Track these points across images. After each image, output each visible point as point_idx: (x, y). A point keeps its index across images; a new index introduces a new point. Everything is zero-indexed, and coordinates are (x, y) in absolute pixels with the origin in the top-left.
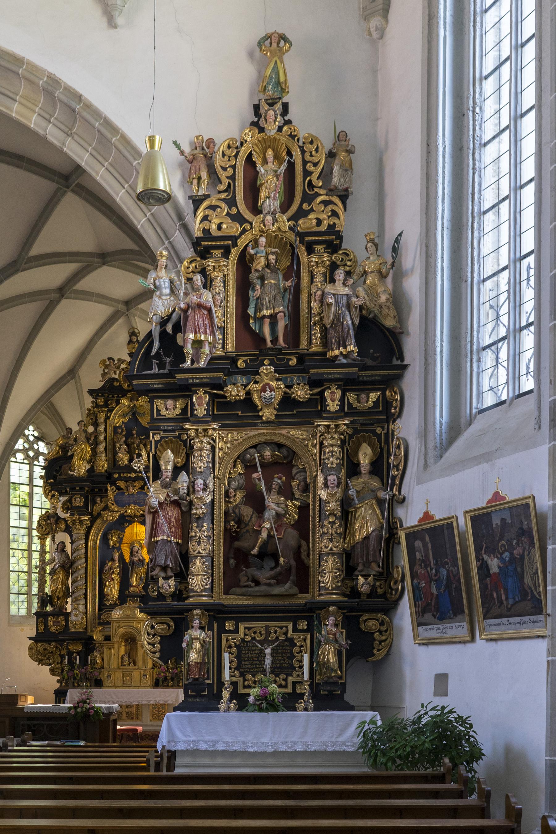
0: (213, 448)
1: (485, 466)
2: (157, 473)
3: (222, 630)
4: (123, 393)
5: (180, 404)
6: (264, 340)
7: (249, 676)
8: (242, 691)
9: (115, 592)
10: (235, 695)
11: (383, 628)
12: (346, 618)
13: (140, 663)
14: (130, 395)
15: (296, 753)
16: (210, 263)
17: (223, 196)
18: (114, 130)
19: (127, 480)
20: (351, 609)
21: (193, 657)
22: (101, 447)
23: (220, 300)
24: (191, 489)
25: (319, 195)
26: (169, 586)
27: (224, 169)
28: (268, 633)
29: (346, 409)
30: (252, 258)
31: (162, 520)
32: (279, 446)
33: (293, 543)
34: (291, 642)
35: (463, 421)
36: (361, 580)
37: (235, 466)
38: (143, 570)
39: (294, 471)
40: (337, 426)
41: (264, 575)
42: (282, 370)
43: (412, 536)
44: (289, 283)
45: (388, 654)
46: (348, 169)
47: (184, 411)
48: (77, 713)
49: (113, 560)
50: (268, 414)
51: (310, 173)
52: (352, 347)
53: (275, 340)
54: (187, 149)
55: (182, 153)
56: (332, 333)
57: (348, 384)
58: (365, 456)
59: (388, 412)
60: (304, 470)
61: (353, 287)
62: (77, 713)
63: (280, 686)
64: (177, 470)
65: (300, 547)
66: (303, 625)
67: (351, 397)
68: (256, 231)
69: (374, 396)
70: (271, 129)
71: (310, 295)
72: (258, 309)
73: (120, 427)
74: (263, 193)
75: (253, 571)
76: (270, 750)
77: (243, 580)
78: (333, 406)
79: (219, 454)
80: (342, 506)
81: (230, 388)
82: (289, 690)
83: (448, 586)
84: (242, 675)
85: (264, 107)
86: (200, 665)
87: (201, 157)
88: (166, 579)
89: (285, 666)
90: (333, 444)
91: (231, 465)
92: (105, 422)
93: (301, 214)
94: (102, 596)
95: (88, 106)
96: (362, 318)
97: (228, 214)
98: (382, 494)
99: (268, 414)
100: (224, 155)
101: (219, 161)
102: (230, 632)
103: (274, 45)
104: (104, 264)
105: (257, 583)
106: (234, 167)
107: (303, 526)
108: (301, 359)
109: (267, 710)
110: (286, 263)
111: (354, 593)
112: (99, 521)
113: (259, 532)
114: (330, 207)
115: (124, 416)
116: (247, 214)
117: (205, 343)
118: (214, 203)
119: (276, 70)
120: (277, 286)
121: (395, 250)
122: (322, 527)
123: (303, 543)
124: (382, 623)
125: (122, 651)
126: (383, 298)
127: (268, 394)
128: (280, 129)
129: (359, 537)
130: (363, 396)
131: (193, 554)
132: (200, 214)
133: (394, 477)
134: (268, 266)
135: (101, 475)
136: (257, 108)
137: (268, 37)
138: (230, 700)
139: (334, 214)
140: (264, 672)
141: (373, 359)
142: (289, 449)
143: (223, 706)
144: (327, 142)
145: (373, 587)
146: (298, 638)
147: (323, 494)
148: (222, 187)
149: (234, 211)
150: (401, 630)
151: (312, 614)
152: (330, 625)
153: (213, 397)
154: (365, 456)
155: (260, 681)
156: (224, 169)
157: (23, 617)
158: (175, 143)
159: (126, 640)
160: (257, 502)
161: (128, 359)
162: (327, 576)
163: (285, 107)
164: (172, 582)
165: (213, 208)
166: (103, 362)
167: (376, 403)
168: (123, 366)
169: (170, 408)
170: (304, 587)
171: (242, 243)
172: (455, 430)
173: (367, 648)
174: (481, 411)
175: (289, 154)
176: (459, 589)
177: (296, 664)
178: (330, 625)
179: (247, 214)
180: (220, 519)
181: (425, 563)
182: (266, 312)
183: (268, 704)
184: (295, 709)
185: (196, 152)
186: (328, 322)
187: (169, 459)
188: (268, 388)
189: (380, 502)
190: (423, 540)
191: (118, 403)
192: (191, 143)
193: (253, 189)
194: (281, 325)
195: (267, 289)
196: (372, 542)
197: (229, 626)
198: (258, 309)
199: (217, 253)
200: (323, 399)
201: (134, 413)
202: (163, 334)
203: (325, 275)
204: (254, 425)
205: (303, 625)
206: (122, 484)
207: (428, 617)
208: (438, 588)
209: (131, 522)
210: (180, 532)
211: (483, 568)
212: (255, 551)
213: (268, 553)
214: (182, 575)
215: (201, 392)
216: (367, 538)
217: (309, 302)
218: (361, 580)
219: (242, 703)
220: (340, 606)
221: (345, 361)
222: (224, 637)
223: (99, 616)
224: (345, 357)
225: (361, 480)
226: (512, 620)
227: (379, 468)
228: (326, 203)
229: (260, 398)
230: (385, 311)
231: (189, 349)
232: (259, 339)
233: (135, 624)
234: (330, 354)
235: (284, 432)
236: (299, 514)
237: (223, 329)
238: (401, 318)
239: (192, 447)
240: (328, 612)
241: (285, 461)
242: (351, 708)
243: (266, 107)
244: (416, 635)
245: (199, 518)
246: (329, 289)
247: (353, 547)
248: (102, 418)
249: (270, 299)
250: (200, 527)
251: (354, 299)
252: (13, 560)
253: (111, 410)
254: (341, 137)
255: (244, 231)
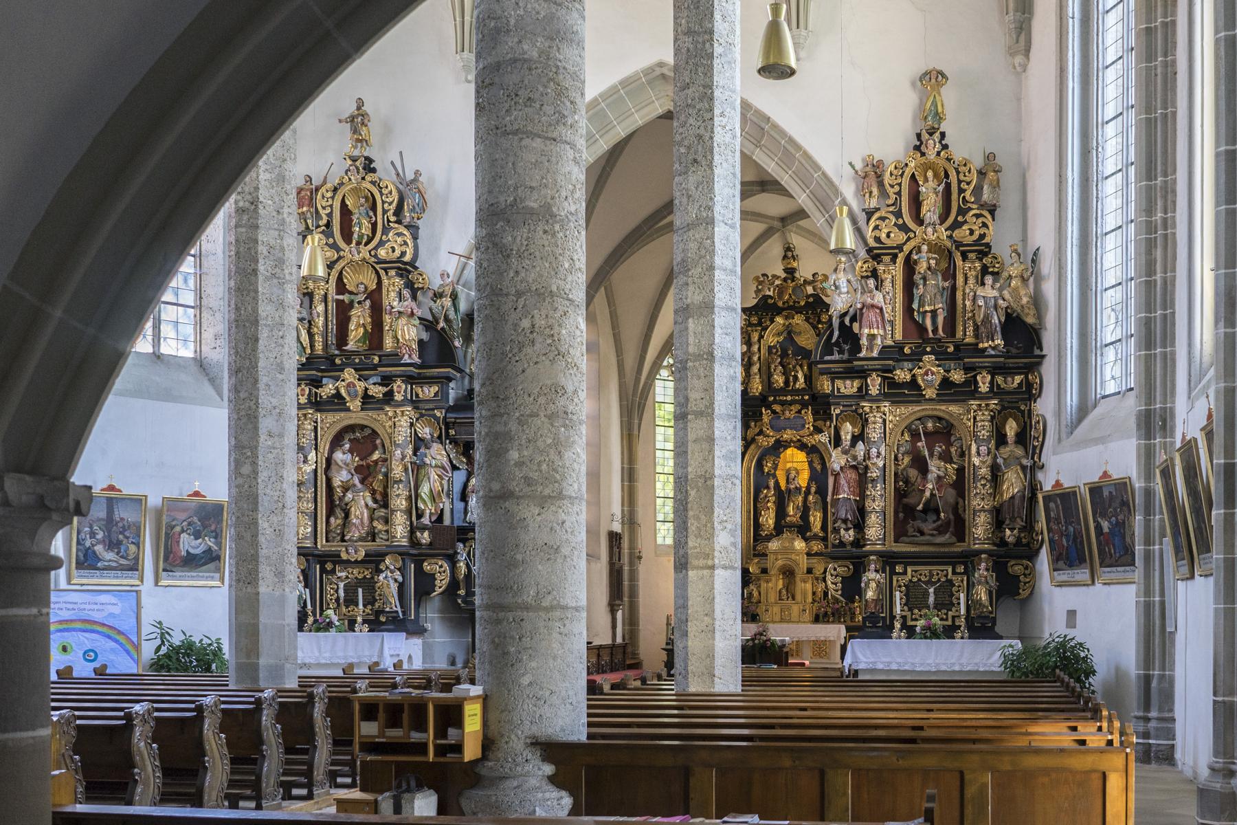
0: (884, 421)
1: (1101, 447)
2: (837, 441)
3: (893, 572)
4: (778, 311)
5: (856, 384)
6: (926, 330)
7: (916, 611)
8: (910, 623)
9: (771, 522)
10: (904, 626)
11: (1027, 572)
12: (995, 563)
13: (799, 597)
14: (785, 313)
15: (954, 672)
16: (881, 268)
17: (891, 209)
18: (798, 147)
19: (783, 403)
20: (1001, 557)
21: (870, 594)
22: (755, 369)
23: (889, 298)
24: (867, 456)
25: (970, 209)
26: (849, 536)
27: (892, 186)
28: (931, 575)
29: (995, 391)
30: (916, 262)
31: (843, 481)
32: (940, 419)
33: (951, 500)
34: (950, 582)
35: (1090, 404)
36: (1008, 532)
37: (902, 434)
38: (800, 499)
39: (953, 438)
40: (987, 405)
41: (928, 527)
42: (941, 356)
43: (1047, 499)
44: (947, 284)
45: (1031, 593)
46: (996, 186)
47: (860, 389)
48: (754, 645)
49: (768, 487)
50: (930, 393)
51: (964, 191)
52: (999, 341)
53: (935, 331)
54: (859, 166)
55: (856, 172)
56: (982, 329)
57: (994, 370)
58: (1011, 428)
59: (1030, 393)
60: (960, 439)
61: (1001, 290)
62: (754, 645)
63: (942, 619)
64: (855, 439)
65: (957, 503)
66: (961, 569)
67: (999, 379)
68: (918, 240)
69: (1018, 379)
70: (931, 154)
71: (964, 294)
72: (921, 305)
73: (775, 347)
74: (924, 209)
75: (919, 523)
76: (934, 669)
77: (911, 531)
78: (984, 388)
79: (889, 426)
80: (992, 471)
81: (898, 372)
82: (949, 623)
83: (1075, 540)
84: (910, 610)
85: (925, 136)
86: (876, 601)
87: (873, 173)
88: (847, 530)
89: (945, 602)
90: (984, 417)
91: (899, 437)
92: (759, 341)
93: (956, 225)
94: (757, 526)
95: (775, 127)
96: (1008, 315)
97: (895, 224)
98: (1025, 462)
99: (930, 393)
100: (891, 174)
101: (887, 179)
102: (899, 574)
103: (933, 80)
104: (763, 191)
105: (922, 534)
106: (900, 184)
107: (960, 485)
108: (957, 347)
109: (931, 638)
110: (944, 265)
111: (1003, 543)
112: (753, 447)
113: (923, 491)
114: (980, 220)
115: (779, 334)
116: (911, 225)
117: (876, 335)
118: (884, 214)
119: (934, 104)
120: (937, 285)
121: (1033, 261)
122: (976, 488)
123: (960, 500)
124: (1026, 568)
125: (780, 584)
126: (1025, 300)
127: (930, 378)
128: (938, 154)
129: (1006, 496)
130: (1009, 379)
131: (869, 509)
132: (872, 224)
133: (1035, 447)
134: (929, 268)
135: (754, 397)
136: (919, 136)
137: (926, 74)
138: (901, 630)
139: (985, 225)
140: (928, 608)
141: (1018, 348)
142: (947, 421)
143: (895, 635)
144: (978, 162)
145: (1019, 539)
146: (957, 580)
147: (976, 461)
148: (890, 202)
149: (900, 221)
150: (1041, 574)
151: (968, 560)
152: (982, 571)
153: (884, 378)
154: (1011, 428)
155: (926, 615)
156: (892, 186)
157: (669, 546)
158: (850, 164)
159: (784, 573)
160: (921, 465)
161: (783, 275)
162: (980, 528)
163: (943, 135)
164: (851, 532)
165: (883, 219)
166: (757, 278)
167: (1020, 384)
168: (777, 282)
169: (849, 387)
170: (961, 539)
171: (907, 249)
172: (1083, 410)
173: (1013, 588)
174: (1104, 397)
175: (947, 176)
176: (1082, 542)
177: (955, 601)
178: (982, 571)
179: (911, 225)
180: (891, 479)
181: (1057, 520)
182: (927, 308)
183: (931, 633)
184: (953, 638)
185: (868, 169)
186: (979, 319)
187: (848, 430)
188: (930, 372)
189: (1024, 468)
190: (1056, 503)
191: (772, 321)
192: (864, 160)
193: (916, 202)
194: (940, 320)
195: (929, 288)
196: (1017, 501)
197: (899, 569)
198: (921, 305)
199: (887, 259)
200: (976, 382)
201: (789, 333)
202: (842, 324)
203: (977, 277)
204: (919, 402)
205: (961, 569)
206: (777, 408)
207: (1061, 564)
208: (1068, 541)
209: (786, 448)
210: (857, 491)
211: (1098, 528)
212: (920, 507)
213: (931, 508)
214: (860, 526)
215: (874, 375)
216: (1013, 497)
217: (964, 300)
218: (1008, 532)
219: (910, 633)
220: (990, 553)
221: (993, 353)
222: (895, 578)
223: (755, 547)
224: (994, 348)
225: (1008, 449)
226: (1119, 569)
227: (1022, 438)
228: (977, 216)
229: (923, 380)
230: (1026, 311)
231: (864, 341)
232: (922, 329)
233: (793, 557)
234: (981, 345)
235: (943, 408)
236: (957, 475)
237: (892, 323)
238: (1040, 316)
239: (867, 420)
240: (980, 559)
241: (944, 432)
242: (1001, 638)
243: (927, 136)
244: (1052, 579)
245: (873, 480)
246: (980, 292)
247: (1002, 505)
248: (755, 337)
249: (930, 293)
250: (874, 487)
251: (1001, 302)
252: (659, 485)
253: (765, 329)
254: (990, 157)
255: (909, 239)
